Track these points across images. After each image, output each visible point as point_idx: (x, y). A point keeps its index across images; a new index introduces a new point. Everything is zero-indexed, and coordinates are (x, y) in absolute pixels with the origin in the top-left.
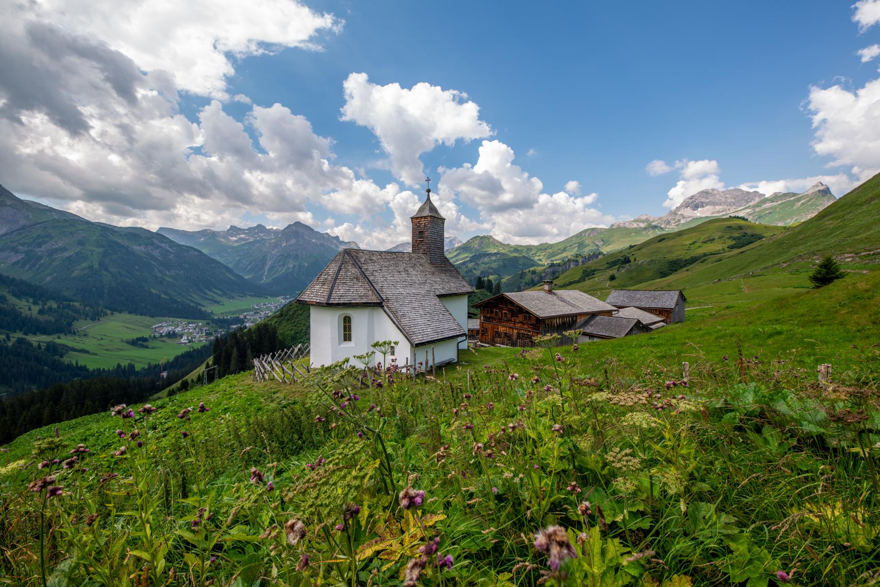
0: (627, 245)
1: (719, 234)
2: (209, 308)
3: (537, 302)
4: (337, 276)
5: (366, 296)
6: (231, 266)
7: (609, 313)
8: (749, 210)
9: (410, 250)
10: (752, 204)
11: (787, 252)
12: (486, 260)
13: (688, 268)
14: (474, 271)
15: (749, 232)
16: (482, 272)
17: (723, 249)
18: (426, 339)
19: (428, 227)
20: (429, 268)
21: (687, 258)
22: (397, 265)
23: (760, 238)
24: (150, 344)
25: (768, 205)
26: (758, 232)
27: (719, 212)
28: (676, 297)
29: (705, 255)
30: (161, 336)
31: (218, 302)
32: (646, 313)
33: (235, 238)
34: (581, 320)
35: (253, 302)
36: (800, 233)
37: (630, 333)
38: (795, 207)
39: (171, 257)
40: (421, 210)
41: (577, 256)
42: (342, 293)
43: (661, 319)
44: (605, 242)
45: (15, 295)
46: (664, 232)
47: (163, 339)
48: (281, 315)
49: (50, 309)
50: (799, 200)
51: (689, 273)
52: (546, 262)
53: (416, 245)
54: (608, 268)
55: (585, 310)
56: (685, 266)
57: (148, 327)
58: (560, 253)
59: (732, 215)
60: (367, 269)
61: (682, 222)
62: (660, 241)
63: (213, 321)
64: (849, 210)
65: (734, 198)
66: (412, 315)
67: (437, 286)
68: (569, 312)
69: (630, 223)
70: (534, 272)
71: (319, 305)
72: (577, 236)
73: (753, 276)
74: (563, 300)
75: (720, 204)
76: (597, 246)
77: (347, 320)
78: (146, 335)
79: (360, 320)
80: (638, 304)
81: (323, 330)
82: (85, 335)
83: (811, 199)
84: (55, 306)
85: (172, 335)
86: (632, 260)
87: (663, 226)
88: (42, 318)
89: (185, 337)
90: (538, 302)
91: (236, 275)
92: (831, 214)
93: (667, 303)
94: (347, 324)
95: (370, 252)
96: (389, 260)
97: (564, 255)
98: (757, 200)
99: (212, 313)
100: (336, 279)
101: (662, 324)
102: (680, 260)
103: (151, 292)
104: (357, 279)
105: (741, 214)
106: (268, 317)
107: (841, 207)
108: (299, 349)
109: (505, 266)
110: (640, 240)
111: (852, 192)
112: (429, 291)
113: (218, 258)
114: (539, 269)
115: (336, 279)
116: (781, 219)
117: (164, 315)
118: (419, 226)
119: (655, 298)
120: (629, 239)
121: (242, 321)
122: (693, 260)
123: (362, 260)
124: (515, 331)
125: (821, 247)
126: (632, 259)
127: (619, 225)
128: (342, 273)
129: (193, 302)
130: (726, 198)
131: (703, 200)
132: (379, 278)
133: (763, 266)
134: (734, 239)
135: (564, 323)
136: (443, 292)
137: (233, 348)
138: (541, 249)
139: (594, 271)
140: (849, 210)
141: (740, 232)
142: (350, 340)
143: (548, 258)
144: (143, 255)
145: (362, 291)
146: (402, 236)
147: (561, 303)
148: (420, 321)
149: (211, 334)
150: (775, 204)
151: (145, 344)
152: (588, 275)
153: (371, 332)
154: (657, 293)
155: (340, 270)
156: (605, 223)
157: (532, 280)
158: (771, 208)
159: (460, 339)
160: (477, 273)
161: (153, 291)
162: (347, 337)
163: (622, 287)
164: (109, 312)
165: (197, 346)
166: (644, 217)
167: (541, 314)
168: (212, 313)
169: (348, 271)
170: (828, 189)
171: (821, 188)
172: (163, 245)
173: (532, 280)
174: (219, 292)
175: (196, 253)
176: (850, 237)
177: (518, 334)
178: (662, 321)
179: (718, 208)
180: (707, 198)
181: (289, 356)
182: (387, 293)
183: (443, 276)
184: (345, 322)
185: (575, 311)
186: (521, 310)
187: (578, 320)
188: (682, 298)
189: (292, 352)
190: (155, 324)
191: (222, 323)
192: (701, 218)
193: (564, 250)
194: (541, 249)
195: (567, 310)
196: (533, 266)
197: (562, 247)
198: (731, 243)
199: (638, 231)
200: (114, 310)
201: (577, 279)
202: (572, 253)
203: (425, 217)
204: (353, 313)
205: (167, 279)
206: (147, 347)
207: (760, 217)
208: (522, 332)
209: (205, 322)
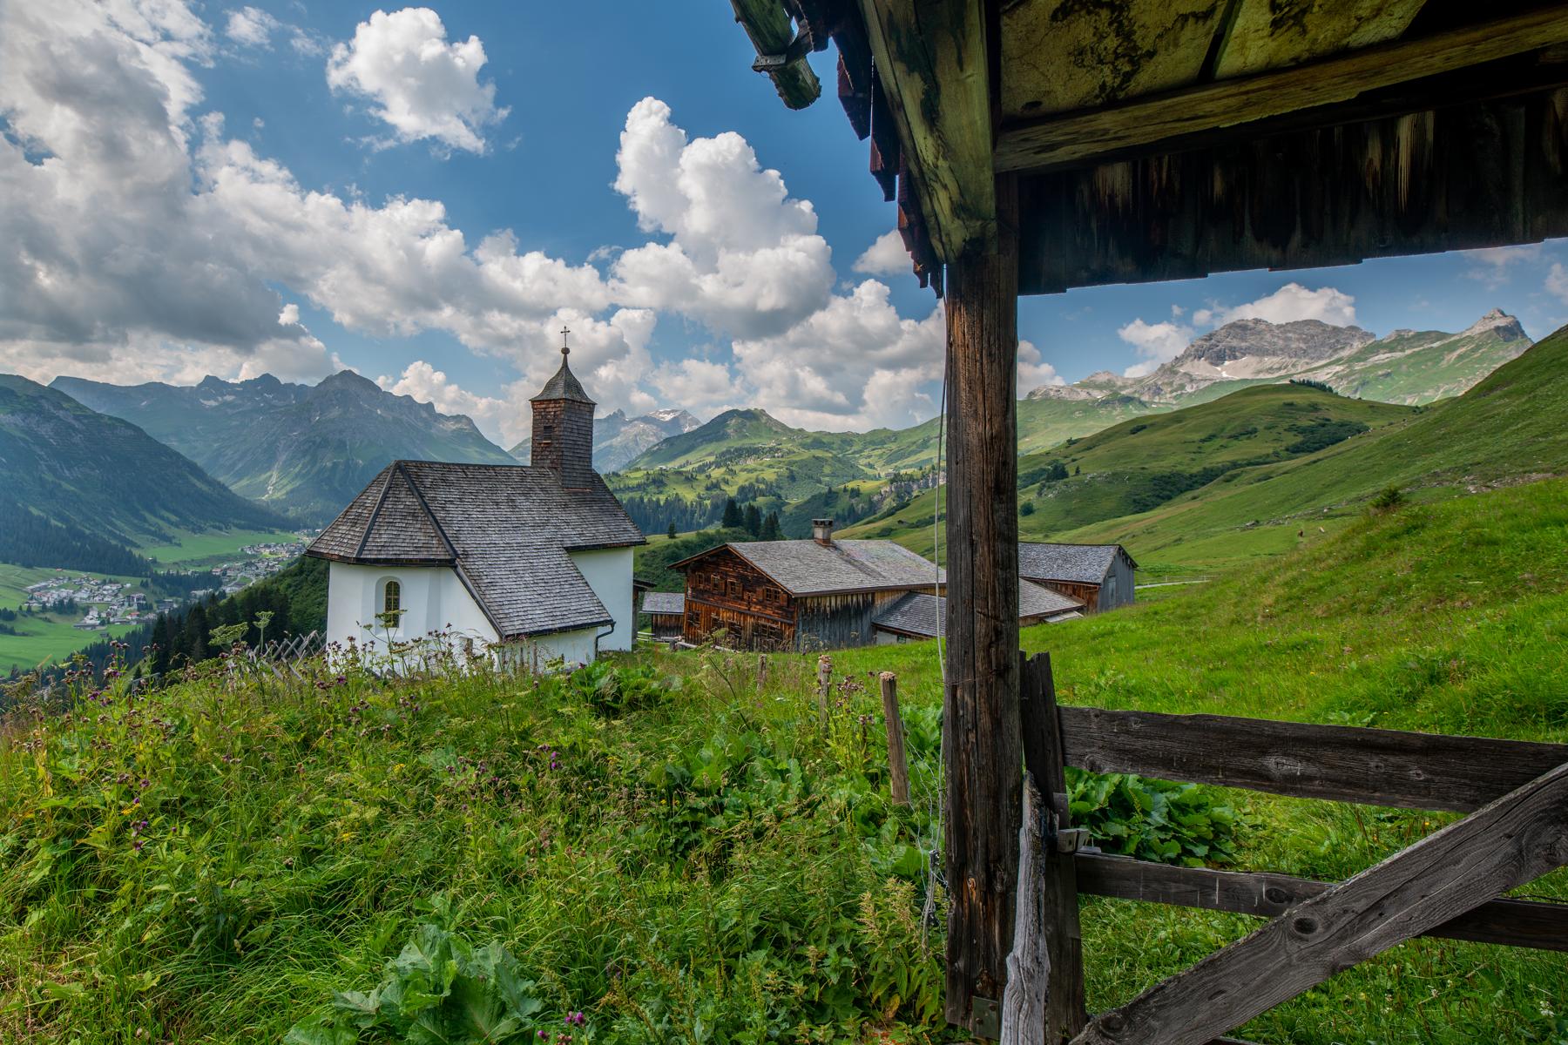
0: (1063, 439)
1: (1267, 420)
2: (150, 551)
3: (795, 562)
4: (379, 509)
5: (427, 547)
6: (200, 462)
8: (1339, 368)
9: (526, 460)
10: (1345, 353)
11: (1407, 466)
12: (751, 463)
14: (724, 487)
15: (1335, 416)
16: (742, 489)
17: (1276, 454)
18: (529, 628)
19: (564, 415)
20: (557, 495)
22: (493, 491)
23: (1359, 430)
24: (20, 627)
25: (1382, 357)
28: (1110, 559)
29: (1235, 465)
30: (44, 609)
31: (168, 539)
33: (213, 403)
34: (881, 603)
35: (236, 542)
36: (1439, 422)
38: (1444, 364)
39: (77, 439)
40: (551, 386)
42: (385, 541)
46: (1148, 412)
47: (48, 615)
48: (301, 571)
50: (1451, 347)
51: (1196, 505)
52: (885, 471)
55: (894, 581)
56: (1190, 488)
57: (17, 587)
58: (915, 452)
59: (1296, 378)
61: (1189, 389)
62: (1134, 432)
63: (156, 579)
64: (1546, 376)
65: (1305, 341)
66: (507, 584)
67: (568, 531)
68: (856, 586)
69: (1072, 389)
70: (856, 493)
71: (344, 560)
73: (1327, 517)
74: (850, 560)
75: (1274, 354)
77: (393, 590)
78: (12, 606)
79: (416, 590)
81: (350, 606)
83: (1478, 347)
85: (67, 608)
86: (1072, 473)
87: (1145, 398)
89: (94, 613)
90: (796, 566)
91: (213, 483)
92: (1508, 384)
93: (1090, 572)
95: (444, 465)
96: (480, 482)
97: (923, 456)
98: (1357, 345)
99: (154, 561)
101: (1075, 614)
102: (1179, 474)
103: (28, 513)
104: (414, 516)
105: (1321, 377)
106: (272, 574)
107: (1530, 368)
108: (312, 642)
109: (792, 477)
110: (1090, 428)
111: (1553, 337)
112: (550, 540)
113: (174, 444)
114: (866, 486)
115: (377, 515)
116: (1414, 389)
117: (53, 565)
118: (544, 417)
120: (1068, 425)
121: (216, 581)
122: (1208, 476)
123: (428, 482)
124: (750, 620)
125: (1481, 456)
126: (1071, 471)
127: (1046, 394)
129: (116, 537)
130: (1287, 339)
131: (1235, 343)
133: (1354, 494)
135: (846, 608)
136: (580, 542)
137: (194, 640)
138: (872, 443)
140: (1546, 376)
141: (1313, 415)
142: (396, 625)
143: (888, 462)
144: (18, 434)
145: (421, 538)
146: (510, 431)
147: (844, 566)
148: (523, 595)
149: (149, 608)
150: (1398, 355)
151: (8, 625)
153: (435, 608)
154: (1072, 550)
157: (852, 510)
158: (1389, 364)
159: (601, 630)
160: (732, 491)
161: (35, 511)
165: (118, 632)
166: (1102, 378)
167: (796, 587)
168: (154, 561)
169: (398, 500)
170: (1518, 324)
171: (1501, 322)
172: (61, 413)
174: (174, 518)
175: (130, 432)
176: (1545, 435)
177: (756, 628)
178: (1079, 609)
179: (1269, 361)
180: (1243, 340)
181: (292, 653)
182: (468, 541)
183: (585, 511)
184: (388, 593)
185: (869, 583)
186: (762, 580)
187: (878, 602)
188: (1125, 560)
189: (297, 646)
190: (32, 581)
191: (175, 584)
192: (1231, 382)
195: (853, 580)
196: (854, 478)
197: (918, 437)
198: (1293, 439)
199: (1089, 408)
203: (556, 401)
204: (402, 577)
205: (65, 485)
206: (12, 632)
207: (1364, 384)
208: (762, 622)
209: (138, 580)
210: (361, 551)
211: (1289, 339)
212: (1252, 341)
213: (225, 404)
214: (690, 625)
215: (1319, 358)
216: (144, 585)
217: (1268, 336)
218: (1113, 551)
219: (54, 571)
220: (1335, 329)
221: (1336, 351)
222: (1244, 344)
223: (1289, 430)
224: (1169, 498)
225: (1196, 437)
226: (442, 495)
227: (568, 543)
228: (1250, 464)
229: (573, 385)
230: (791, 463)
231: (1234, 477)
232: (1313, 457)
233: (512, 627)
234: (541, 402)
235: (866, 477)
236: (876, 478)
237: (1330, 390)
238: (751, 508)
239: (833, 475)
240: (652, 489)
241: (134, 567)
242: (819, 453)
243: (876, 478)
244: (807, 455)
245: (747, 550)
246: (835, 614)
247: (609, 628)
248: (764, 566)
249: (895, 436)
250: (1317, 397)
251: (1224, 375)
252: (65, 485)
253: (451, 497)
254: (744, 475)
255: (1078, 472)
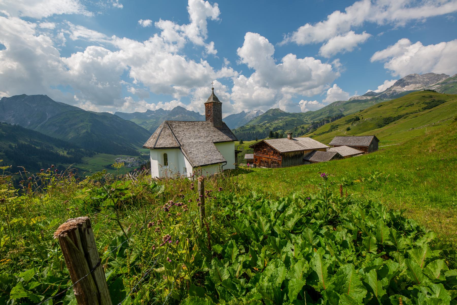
1: (417, 101)
3: (281, 144)
5: (172, 143)
6: (148, 130)
7: (324, 149)
13: (395, 122)
15: (437, 99)
16: (274, 128)
17: (419, 110)
18: (200, 164)
19: (214, 106)
20: (213, 128)
21: (395, 116)
26: (442, 99)
27: (418, 87)
28: (372, 139)
29: (407, 114)
32: (352, 149)
33: (149, 116)
37: (333, 158)
41: (328, 117)
43: (361, 152)
44: (346, 109)
45: (56, 146)
49: (71, 152)
52: (310, 122)
53: (207, 117)
54: (346, 124)
55: (309, 148)
56: (394, 121)
58: (318, 116)
59: (426, 89)
60: (175, 131)
65: (429, 79)
68: (299, 149)
72: (329, 106)
73: (433, 126)
76: (341, 111)
77: (165, 157)
80: (348, 144)
82: (87, 164)
84: (73, 150)
88: (68, 156)
89: (129, 164)
94: (165, 157)
96: (189, 126)
98: (444, 79)
100: (159, 136)
109: (287, 125)
113: (143, 126)
115: (159, 136)
119: (359, 141)
122: (399, 117)
123: (174, 126)
124: (270, 160)
126: (361, 118)
128: (162, 133)
131: (408, 81)
132: (181, 135)
133: (442, 119)
134: (427, 103)
136: (218, 141)
139: (337, 126)
143: (311, 120)
145: (171, 141)
147: (295, 145)
152: (334, 128)
155: (161, 131)
156: (347, 97)
157: (302, 132)
159: (223, 164)
160: (271, 129)
161: (115, 143)
162: (166, 163)
163: (354, 134)
164: (96, 153)
167: (281, 151)
173: (302, 132)
178: (362, 153)
180: (411, 80)
186: (272, 148)
187: (305, 154)
193: (321, 114)
194: (307, 115)
196: (303, 124)
197: (320, 113)
198: (424, 106)
200: (98, 152)
201: (327, 130)
202: (326, 116)
203: (210, 103)
204: (168, 152)
210: (155, 145)
211: (424, 79)
212: (413, 80)
213: (152, 116)
214: (255, 162)
215: (433, 83)
216: (139, 158)
217: (418, 78)
218: (373, 137)
219: (121, 156)
220: (438, 75)
221: (438, 81)
222: (411, 81)
223: (423, 103)
224: (388, 124)
225: (396, 107)
226: (177, 130)
227: (214, 141)
228: (411, 113)
229: (215, 98)
230: (286, 121)
231: (407, 117)
232: (430, 110)
233: (196, 164)
234: (207, 103)
235: (306, 124)
236: (309, 124)
237: (436, 92)
238: (276, 133)
239: (297, 124)
240: (252, 130)
241: (137, 154)
242: (293, 118)
243: (309, 124)
244: (290, 119)
245: (269, 141)
246: (293, 157)
247: (225, 163)
248: (273, 146)
249: (313, 113)
250: (432, 94)
251: (405, 90)
252: (121, 137)
253: (180, 130)
254: (275, 125)
255: (363, 118)
